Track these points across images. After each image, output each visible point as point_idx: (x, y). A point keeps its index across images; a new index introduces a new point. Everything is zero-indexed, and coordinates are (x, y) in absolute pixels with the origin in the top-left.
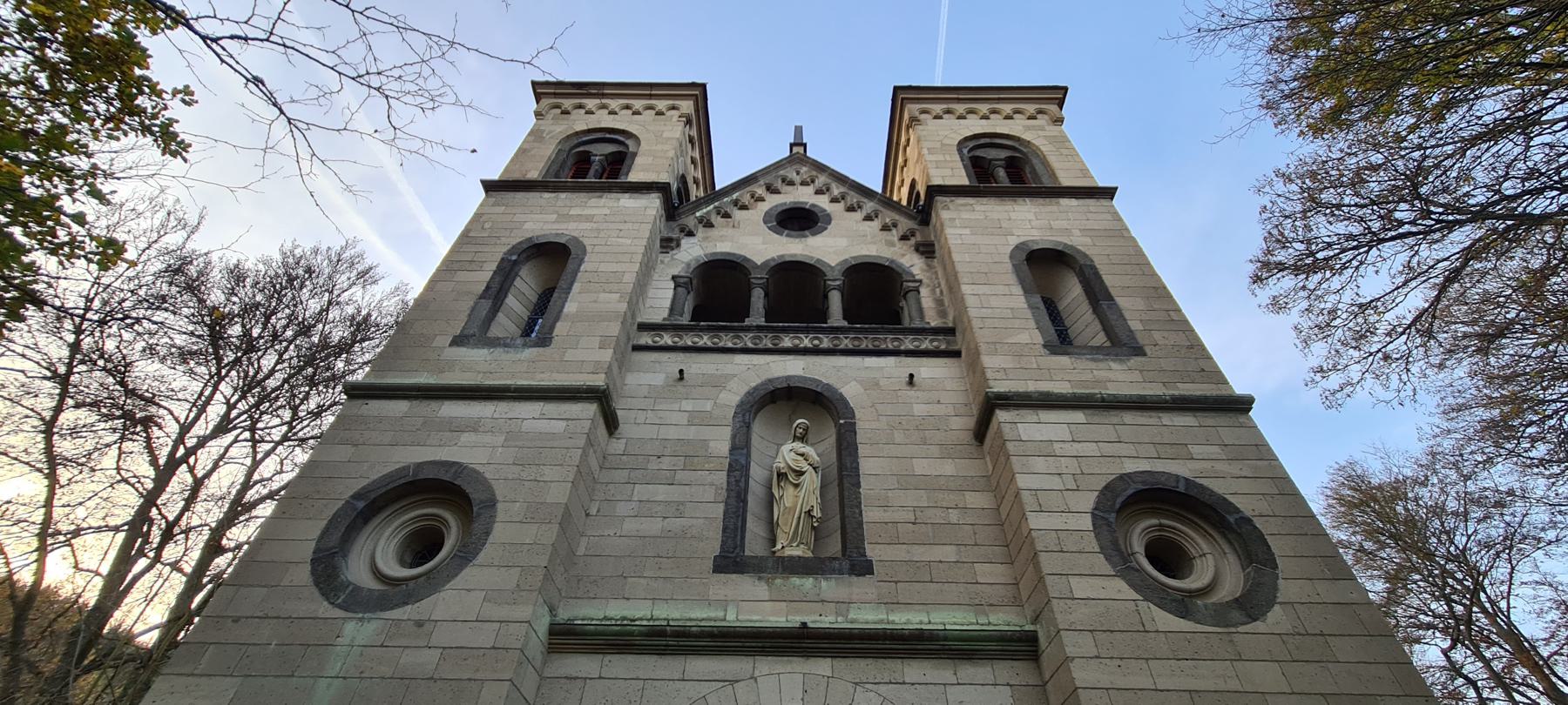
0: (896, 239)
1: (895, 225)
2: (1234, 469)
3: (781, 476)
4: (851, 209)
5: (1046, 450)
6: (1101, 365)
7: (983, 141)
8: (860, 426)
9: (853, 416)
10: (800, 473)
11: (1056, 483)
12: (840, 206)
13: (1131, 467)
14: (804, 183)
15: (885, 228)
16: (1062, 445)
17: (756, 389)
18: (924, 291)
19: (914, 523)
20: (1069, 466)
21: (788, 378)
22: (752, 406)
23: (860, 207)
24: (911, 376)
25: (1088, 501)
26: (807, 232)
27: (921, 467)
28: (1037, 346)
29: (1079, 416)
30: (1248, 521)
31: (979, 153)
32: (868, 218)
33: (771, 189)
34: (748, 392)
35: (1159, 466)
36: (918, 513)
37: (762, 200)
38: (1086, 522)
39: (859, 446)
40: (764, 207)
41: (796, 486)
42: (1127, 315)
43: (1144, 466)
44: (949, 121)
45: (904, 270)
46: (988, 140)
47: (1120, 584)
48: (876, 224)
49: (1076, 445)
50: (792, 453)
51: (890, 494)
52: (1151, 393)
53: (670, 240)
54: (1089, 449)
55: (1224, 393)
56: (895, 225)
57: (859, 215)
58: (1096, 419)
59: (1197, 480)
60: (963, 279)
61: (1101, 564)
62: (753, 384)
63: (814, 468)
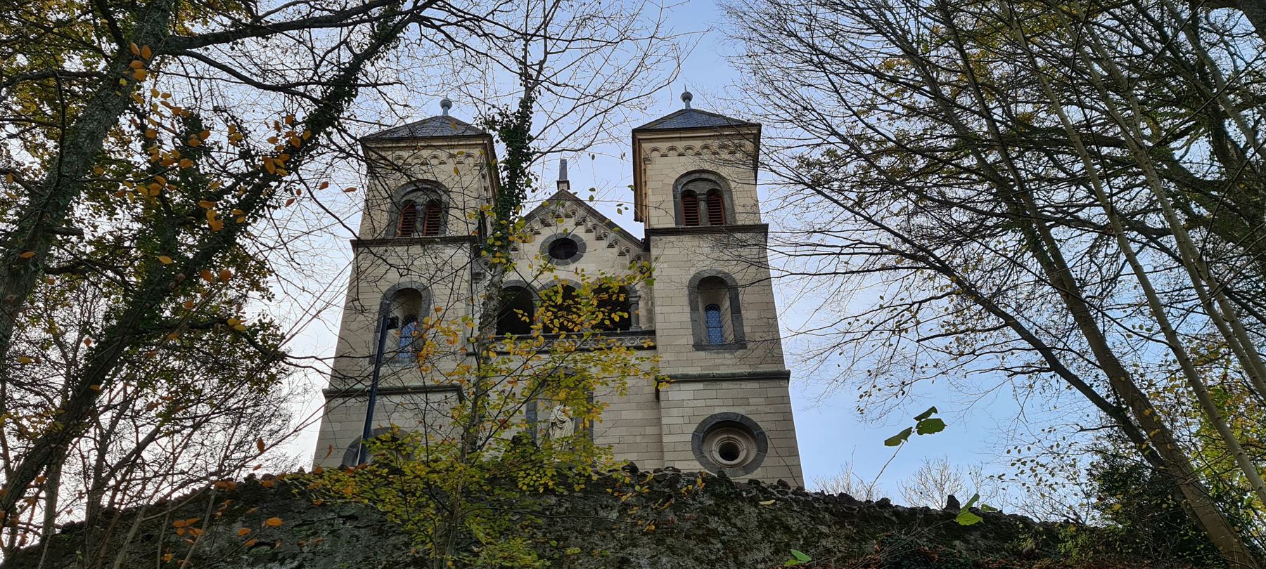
1: (628, 251)
2: (767, 409)
3: (553, 424)
4: (599, 238)
5: (680, 405)
6: (721, 356)
11: (680, 421)
12: (592, 235)
13: (717, 411)
14: (567, 216)
15: (621, 254)
18: (641, 304)
20: (689, 412)
23: (606, 236)
25: (693, 428)
26: (569, 260)
27: (625, 415)
29: (700, 386)
30: (763, 433)
31: (690, 187)
32: (610, 246)
33: (545, 224)
35: (732, 410)
37: (538, 233)
38: (689, 438)
40: (540, 239)
42: (745, 322)
43: (724, 410)
46: (697, 175)
47: (697, 463)
48: (616, 250)
52: (738, 371)
53: (479, 274)
54: (701, 403)
55: (781, 369)
56: (628, 251)
57: (604, 243)
58: (710, 387)
60: (658, 302)
61: (691, 455)
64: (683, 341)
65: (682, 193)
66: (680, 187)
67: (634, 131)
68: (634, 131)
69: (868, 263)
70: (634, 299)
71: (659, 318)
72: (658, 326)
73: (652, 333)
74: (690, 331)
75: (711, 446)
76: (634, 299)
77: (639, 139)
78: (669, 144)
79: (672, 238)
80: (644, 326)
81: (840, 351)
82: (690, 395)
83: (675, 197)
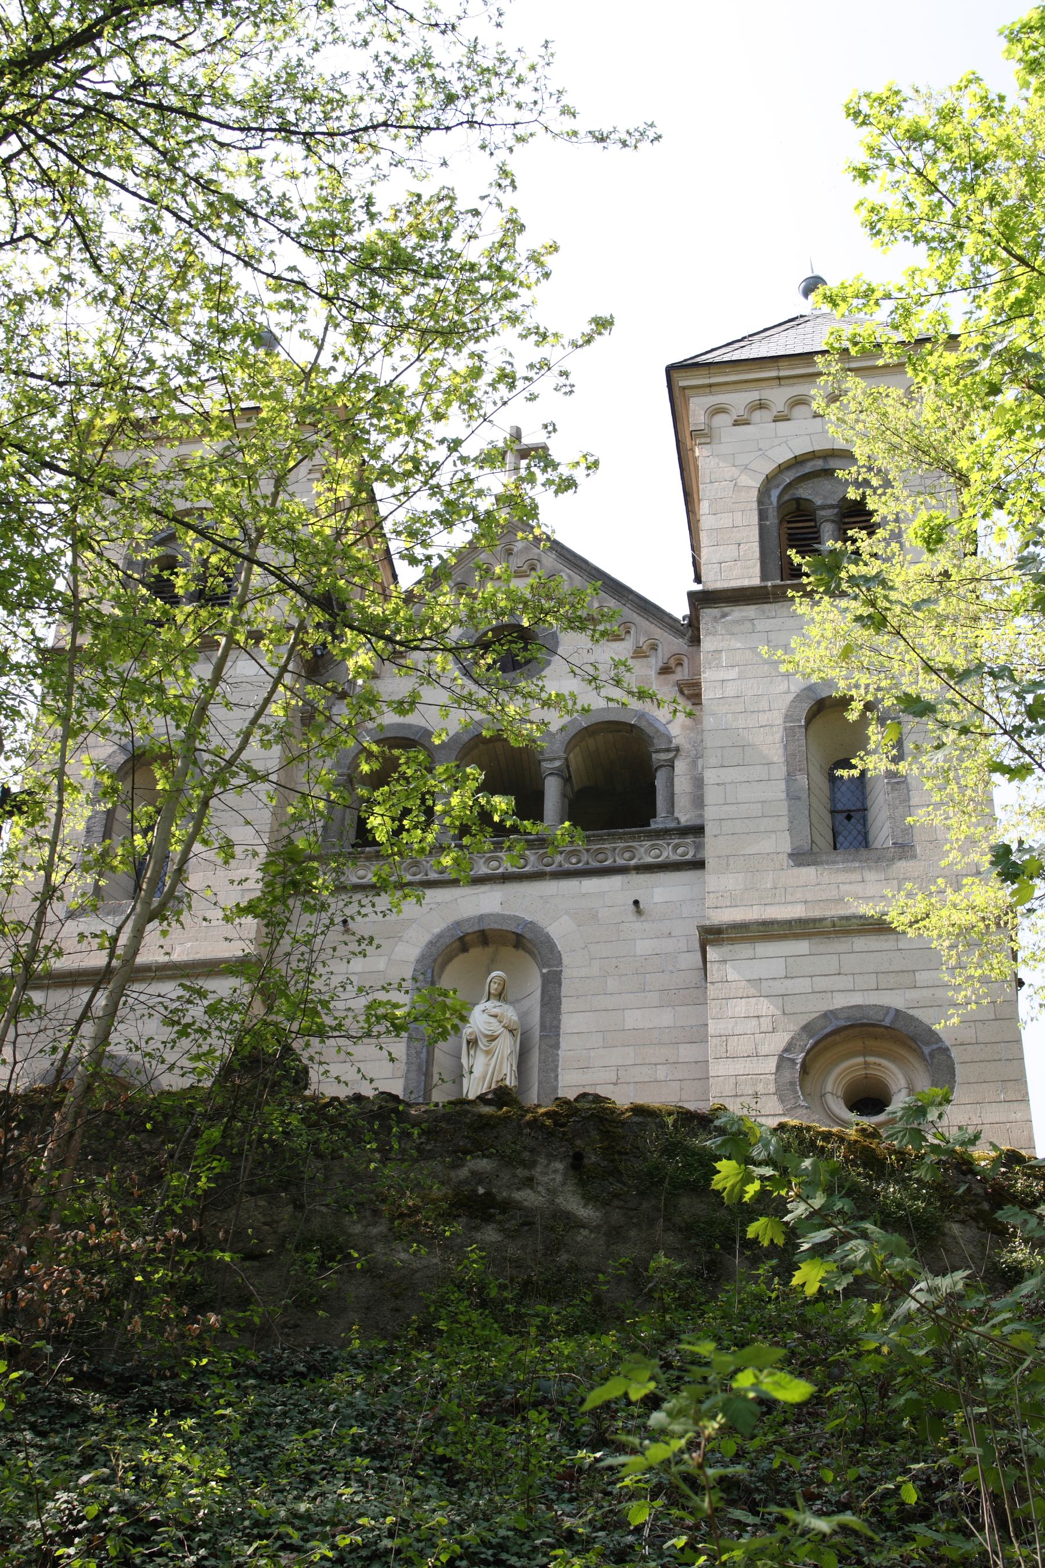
0: (653, 673)
7: (808, 468)
8: (566, 974)
9: (560, 963)
10: (492, 1038)
13: (840, 1001)
16: (771, 983)
17: (440, 936)
19: (615, 1084)
21: (481, 918)
22: (435, 961)
24: (636, 903)
27: (634, 1019)
28: (781, 856)
29: (802, 946)
30: (946, 1051)
34: (431, 942)
36: (621, 1073)
39: (564, 1000)
41: (487, 1053)
43: (856, 999)
44: (762, 427)
45: (658, 731)
49: (787, 982)
50: (485, 1015)
51: (592, 1053)
54: (803, 985)
56: (654, 648)
59: (911, 1012)
62: (437, 930)
63: (510, 1031)
64: (767, 845)
65: (780, 506)
66: (775, 494)
67: (671, 370)
68: (671, 370)
69: (970, 324)
70: (663, 756)
71: (711, 795)
72: (711, 814)
73: (698, 830)
74: (784, 822)
75: (824, 1082)
76: (663, 756)
77: (684, 388)
78: (753, 396)
79: (750, 611)
80: (685, 816)
81: (357, 122)
82: (777, 968)
83: (762, 515)
